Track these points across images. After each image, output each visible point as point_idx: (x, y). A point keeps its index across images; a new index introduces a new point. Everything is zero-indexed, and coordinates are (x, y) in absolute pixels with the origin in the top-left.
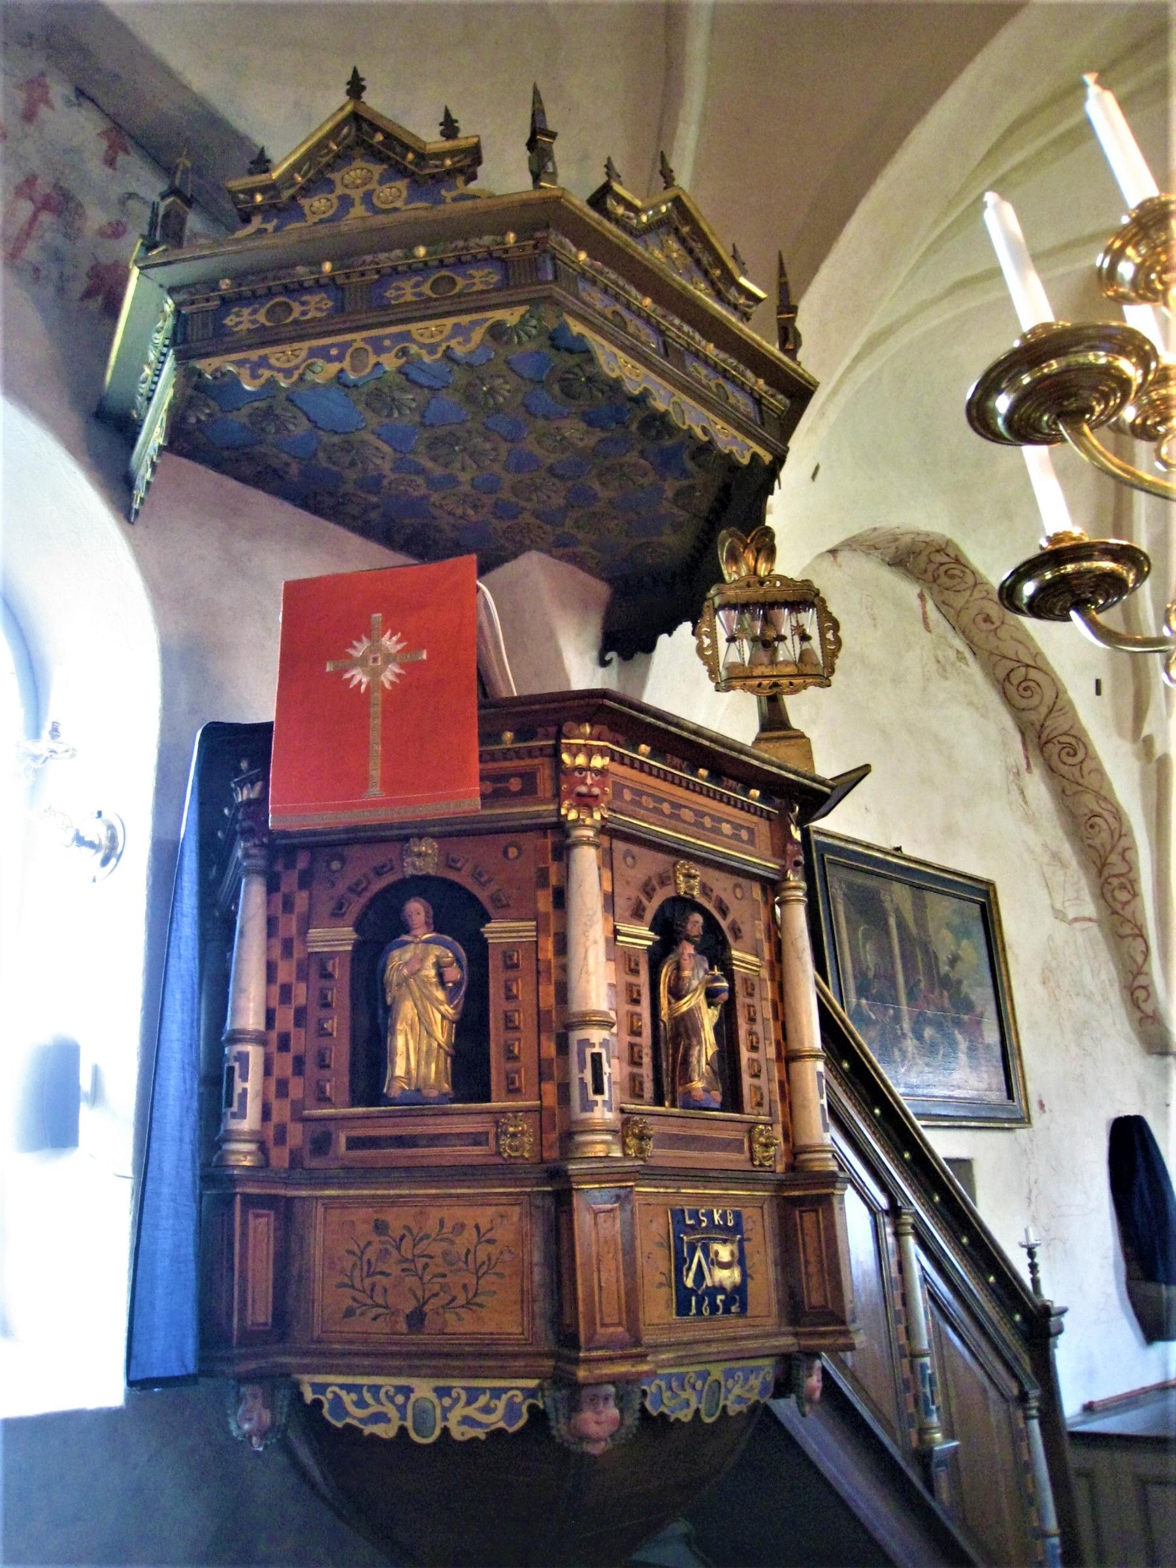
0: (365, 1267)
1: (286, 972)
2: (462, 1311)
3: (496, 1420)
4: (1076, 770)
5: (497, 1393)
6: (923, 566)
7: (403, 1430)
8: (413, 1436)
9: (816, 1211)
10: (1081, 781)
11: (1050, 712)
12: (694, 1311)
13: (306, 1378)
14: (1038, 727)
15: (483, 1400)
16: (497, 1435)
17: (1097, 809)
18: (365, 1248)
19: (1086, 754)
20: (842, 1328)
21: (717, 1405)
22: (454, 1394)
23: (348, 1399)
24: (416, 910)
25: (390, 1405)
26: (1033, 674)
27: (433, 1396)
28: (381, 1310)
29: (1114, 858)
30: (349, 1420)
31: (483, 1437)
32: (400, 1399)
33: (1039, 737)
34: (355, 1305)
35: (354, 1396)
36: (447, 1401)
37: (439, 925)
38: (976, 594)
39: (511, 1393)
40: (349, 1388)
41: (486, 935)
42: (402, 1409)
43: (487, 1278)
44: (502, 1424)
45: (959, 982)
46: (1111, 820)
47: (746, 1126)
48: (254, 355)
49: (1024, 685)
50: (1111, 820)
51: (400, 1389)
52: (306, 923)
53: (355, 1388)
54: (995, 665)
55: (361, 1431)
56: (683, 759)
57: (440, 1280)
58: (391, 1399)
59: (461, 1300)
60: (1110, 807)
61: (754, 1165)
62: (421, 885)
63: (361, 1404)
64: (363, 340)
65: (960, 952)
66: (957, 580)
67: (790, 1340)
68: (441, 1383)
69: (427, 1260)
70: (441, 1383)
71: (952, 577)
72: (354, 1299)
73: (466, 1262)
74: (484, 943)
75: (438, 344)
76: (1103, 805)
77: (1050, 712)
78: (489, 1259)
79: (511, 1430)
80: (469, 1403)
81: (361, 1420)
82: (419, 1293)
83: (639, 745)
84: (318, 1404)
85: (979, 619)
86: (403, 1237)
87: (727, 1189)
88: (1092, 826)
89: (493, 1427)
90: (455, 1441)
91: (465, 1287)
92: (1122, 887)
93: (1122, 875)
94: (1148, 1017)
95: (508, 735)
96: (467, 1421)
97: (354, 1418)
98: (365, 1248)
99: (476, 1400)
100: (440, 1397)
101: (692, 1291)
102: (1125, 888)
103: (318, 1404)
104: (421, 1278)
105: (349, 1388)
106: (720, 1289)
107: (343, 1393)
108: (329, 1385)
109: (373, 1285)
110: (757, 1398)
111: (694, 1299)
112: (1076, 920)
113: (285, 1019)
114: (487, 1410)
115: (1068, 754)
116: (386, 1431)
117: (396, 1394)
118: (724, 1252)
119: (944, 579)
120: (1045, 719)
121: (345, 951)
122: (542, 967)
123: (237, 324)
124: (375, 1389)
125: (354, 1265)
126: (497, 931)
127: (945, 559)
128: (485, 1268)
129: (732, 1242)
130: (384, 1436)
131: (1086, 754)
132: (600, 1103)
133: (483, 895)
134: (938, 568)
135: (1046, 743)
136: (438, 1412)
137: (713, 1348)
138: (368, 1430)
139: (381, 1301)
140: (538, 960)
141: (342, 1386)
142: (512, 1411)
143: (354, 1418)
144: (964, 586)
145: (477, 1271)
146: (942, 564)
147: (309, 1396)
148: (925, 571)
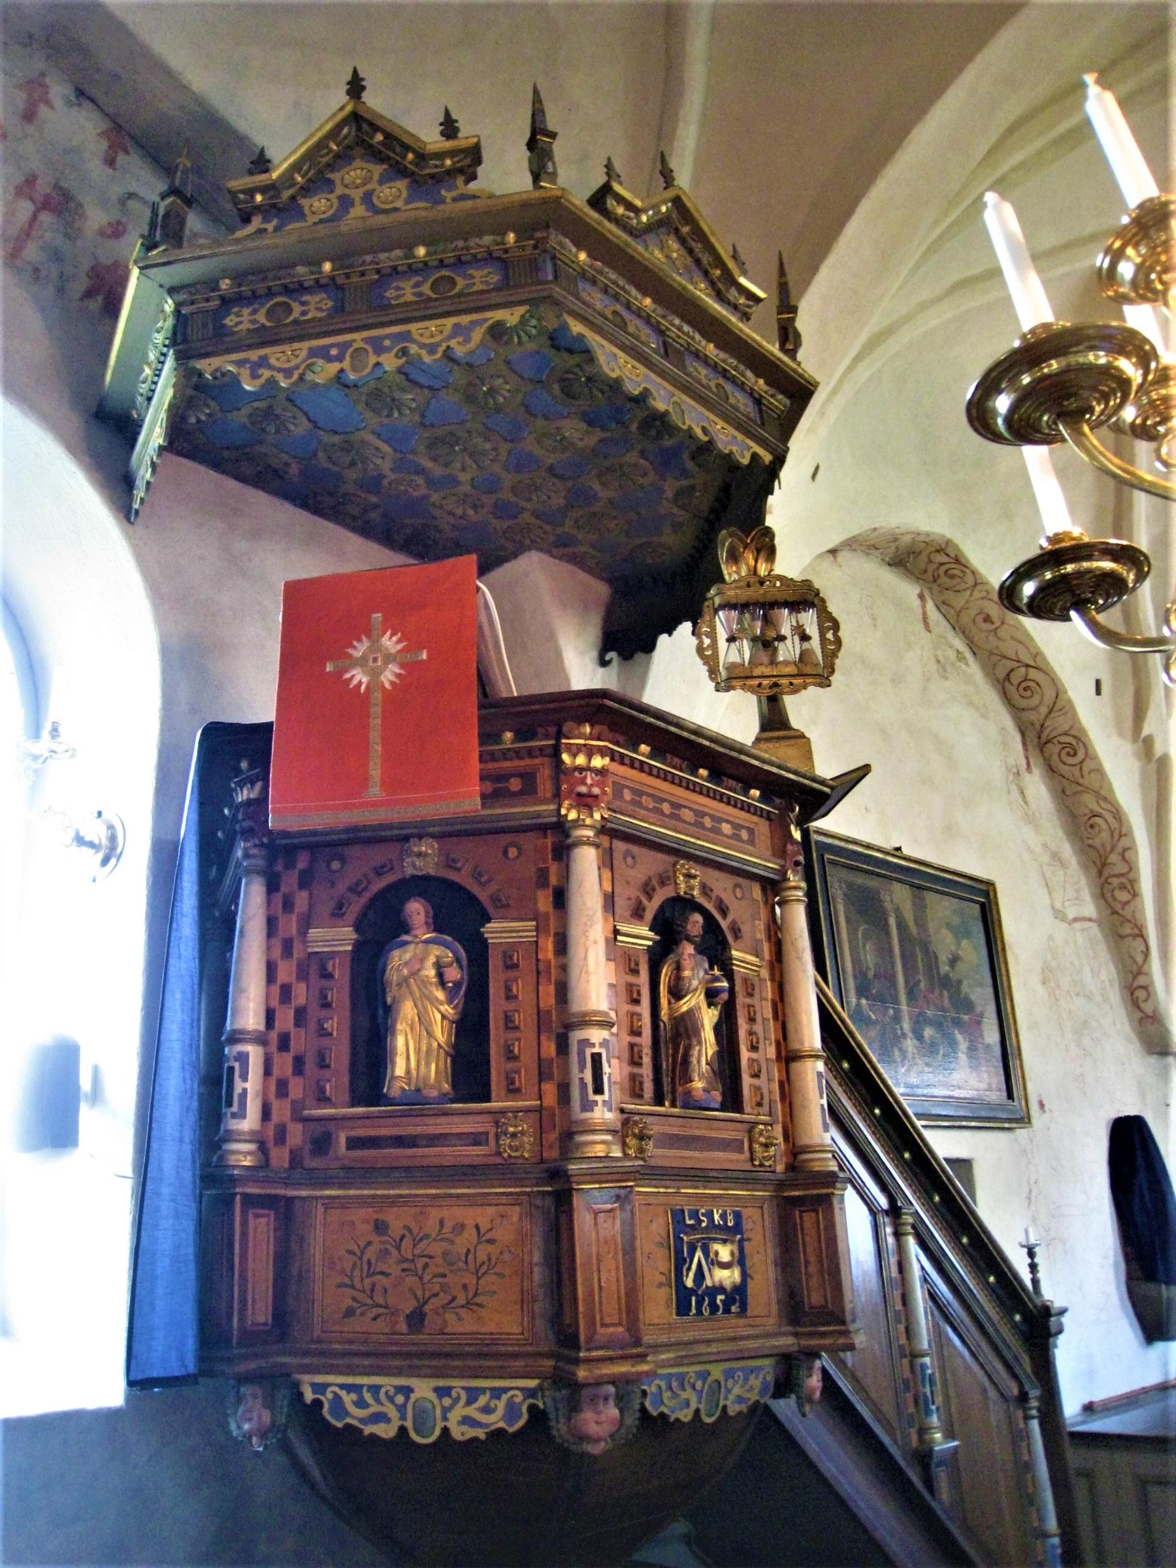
0: (365, 1267)
1: (286, 972)
2: (462, 1311)
3: (496, 1420)
4: (1076, 770)
5: (497, 1393)
6: (923, 566)
7: (403, 1430)
8: (413, 1436)
9: (816, 1211)
10: (1081, 781)
11: (1050, 712)
12: (694, 1311)
13: (306, 1378)
14: (1038, 727)
15: (483, 1400)
16: (497, 1435)
17: (1097, 809)
18: (365, 1248)
19: (1086, 754)
20: (842, 1328)
21: (717, 1405)
22: (454, 1394)
23: (348, 1399)
24: (416, 910)
25: (390, 1405)
26: (1033, 674)
27: (433, 1396)
28: (381, 1310)
29: (1114, 858)
30: (349, 1420)
31: (483, 1437)
32: (400, 1399)
33: (1039, 737)
34: (355, 1305)
35: (354, 1396)
36: (447, 1401)
37: (439, 925)
38: (976, 594)
39: (511, 1393)
40: (349, 1388)
41: (486, 935)
42: (402, 1409)
43: (487, 1278)
44: (502, 1424)
45: (959, 982)
46: (1111, 820)
47: (746, 1126)
48: (254, 355)
49: (1024, 685)
50: (1111, 820)
51: (400, 1389)
52: (306, 923)
53: (355, 1388)
54: (995, 665)
55: (361, 1431)
56: (683, 759)
57: (440, 1280)
58: (391, 1399)
59: (461, 1300)
60: (1110, 807)
61: (754, 1165)
62: (421, 885)
63: (361, 1404)
64: (363, 340)
65: (960, 952)
66: (957, 580)
67: (790, 1340)
68: (441, 1383)
69: (427, 1260)
70: (441, 1383)
71: (952, 577)
72: (354, 1299)
73: (466, 1262)
74: (484, 943)
75: (438, 344)
76: (1103, 805)
77: (1050, 712)
78: (489, 1259)
79: (511, 1430)
80: (469, 1403)
81: (361, 1420)
82: (419, 1293)
83: (639, 745)
84: (318, 1404)
85: (979, 619)
86: (403, 1237)
87: (727, 1189)
88: (1092, 826)
89: (493, 1427)
90: (455, 1441)
91: (465, 1287)
92: (1122, 887)
93: (1122, 875)
94: (1148, 1017)
95: (508, 735)
96: (467, 1421)
97: (354, 1418)
98: (365, 1248)
99: (476, 1400)
100: (440, 1397)
101: (692, 1291)
102: (1125, 888)
103: (318, 1404)
104: (421, 1278)
105: (349, 1388)
106: (720, 1289)
107: (343, 1393)
108: (329, 1385)
109: (373, 1285)
110: (757, 1398)
111: (694, 1299)
112: (1076, 920)
113: (285, 1019)
114: (487, 1410)
115: (1068, 754)
116: (386, 1431)
117: (396, 1394)
118: (724, 1252)
119: (944, 579)
120: (1045, 719)
121: (345, 951)
122: (542, 967)
123: (237, 324)
124: (375, 1389)
125: (354, 1265)
126: (497, 931)
127: (945, 559)
128: (485, 1268)
129: (732, 1242)
130: (384, 1436)
131: (1086, 754)
132: (600, 1103)
133: (483, 895)
134: (938, 568)
135: (1046, 743)
136: (438, 1412)
137: (713, 1348)
138: (368, 1430)
139: (381, 1301)
140: (538, 960)
141: (342, 1386)
142: (512, 1411)
143: (354, 1418)
144: (964, 586)
145: (477, 1271)
146: (942, 564)
147: (309, 1396)
148: (925, 571)
